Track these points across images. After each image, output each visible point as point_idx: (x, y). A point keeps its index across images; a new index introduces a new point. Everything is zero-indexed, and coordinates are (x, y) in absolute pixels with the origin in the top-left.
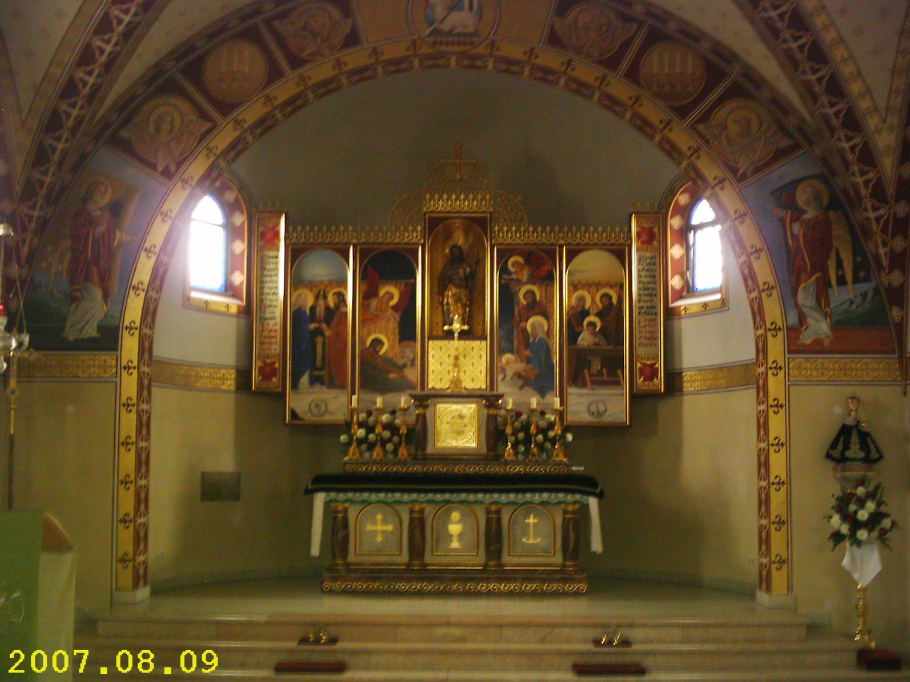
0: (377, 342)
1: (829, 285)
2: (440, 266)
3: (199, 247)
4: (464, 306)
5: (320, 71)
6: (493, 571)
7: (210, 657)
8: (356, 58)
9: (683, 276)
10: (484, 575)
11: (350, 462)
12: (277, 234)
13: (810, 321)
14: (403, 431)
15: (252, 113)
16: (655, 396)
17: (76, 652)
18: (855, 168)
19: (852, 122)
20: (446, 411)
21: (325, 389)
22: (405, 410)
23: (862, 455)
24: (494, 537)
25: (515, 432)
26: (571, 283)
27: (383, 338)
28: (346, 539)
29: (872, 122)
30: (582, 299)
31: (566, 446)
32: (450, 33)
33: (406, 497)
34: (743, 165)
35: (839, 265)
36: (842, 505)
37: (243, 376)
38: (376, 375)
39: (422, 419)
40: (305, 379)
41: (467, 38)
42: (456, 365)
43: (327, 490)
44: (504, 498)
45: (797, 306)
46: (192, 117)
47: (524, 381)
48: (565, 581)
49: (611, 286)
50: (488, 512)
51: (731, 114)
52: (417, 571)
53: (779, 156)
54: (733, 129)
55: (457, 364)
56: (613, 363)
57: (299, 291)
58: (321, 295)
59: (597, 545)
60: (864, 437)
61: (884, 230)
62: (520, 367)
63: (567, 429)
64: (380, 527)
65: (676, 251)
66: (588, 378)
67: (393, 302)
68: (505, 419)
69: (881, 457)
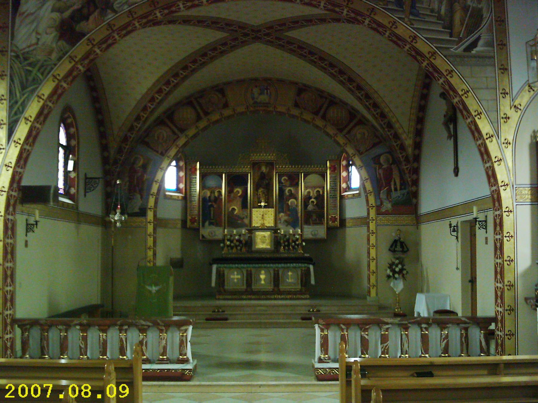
2: (256, 180)
3: (170, 178)
4: (266, 195)
5: (215, 117)
6: (277, 290)
7: (124, 389)
8: (227, 112)
9: (347, 183)
10: (273, 292)
12: (196, 170)
14: (244, 242)
15: (191, 132)
16: (336, 228)
18: (399, 152)
19: (396, 136)
20: (259, 234)
21: (214, 227)
23: (401, 249)
24: (276, 279)
25: (284, 242)
26: (305, 187)
27: (236, 208)
28: (224, 281)
29: (404, 136)
30: (309, 192)
31: (303, 247)
33: (245, 266)
35: (395, 184)
36: (391, 266)
37: (184, 222)
38: (233, 222)
40: (207, 223)
41: (266, 105)
43: (218, 263)
44: (280, 266)
45: (380, 198)
47: (288, 223)
48: (302, 294)
49: (320, 188)
50: (274, 270)
51: (359, 132)
52: (250, 291)
53: (375, 145)
54: (359, 136)
55: (263, 217)
56: (321, 216)
57: (205, 191)
58: (212, 192)
59: (313, 282)
60: (402, 244)
61: (409, 173)
64: (236, 277)
65: (344, 174)
66: (311, 222)
67: (239, 195)
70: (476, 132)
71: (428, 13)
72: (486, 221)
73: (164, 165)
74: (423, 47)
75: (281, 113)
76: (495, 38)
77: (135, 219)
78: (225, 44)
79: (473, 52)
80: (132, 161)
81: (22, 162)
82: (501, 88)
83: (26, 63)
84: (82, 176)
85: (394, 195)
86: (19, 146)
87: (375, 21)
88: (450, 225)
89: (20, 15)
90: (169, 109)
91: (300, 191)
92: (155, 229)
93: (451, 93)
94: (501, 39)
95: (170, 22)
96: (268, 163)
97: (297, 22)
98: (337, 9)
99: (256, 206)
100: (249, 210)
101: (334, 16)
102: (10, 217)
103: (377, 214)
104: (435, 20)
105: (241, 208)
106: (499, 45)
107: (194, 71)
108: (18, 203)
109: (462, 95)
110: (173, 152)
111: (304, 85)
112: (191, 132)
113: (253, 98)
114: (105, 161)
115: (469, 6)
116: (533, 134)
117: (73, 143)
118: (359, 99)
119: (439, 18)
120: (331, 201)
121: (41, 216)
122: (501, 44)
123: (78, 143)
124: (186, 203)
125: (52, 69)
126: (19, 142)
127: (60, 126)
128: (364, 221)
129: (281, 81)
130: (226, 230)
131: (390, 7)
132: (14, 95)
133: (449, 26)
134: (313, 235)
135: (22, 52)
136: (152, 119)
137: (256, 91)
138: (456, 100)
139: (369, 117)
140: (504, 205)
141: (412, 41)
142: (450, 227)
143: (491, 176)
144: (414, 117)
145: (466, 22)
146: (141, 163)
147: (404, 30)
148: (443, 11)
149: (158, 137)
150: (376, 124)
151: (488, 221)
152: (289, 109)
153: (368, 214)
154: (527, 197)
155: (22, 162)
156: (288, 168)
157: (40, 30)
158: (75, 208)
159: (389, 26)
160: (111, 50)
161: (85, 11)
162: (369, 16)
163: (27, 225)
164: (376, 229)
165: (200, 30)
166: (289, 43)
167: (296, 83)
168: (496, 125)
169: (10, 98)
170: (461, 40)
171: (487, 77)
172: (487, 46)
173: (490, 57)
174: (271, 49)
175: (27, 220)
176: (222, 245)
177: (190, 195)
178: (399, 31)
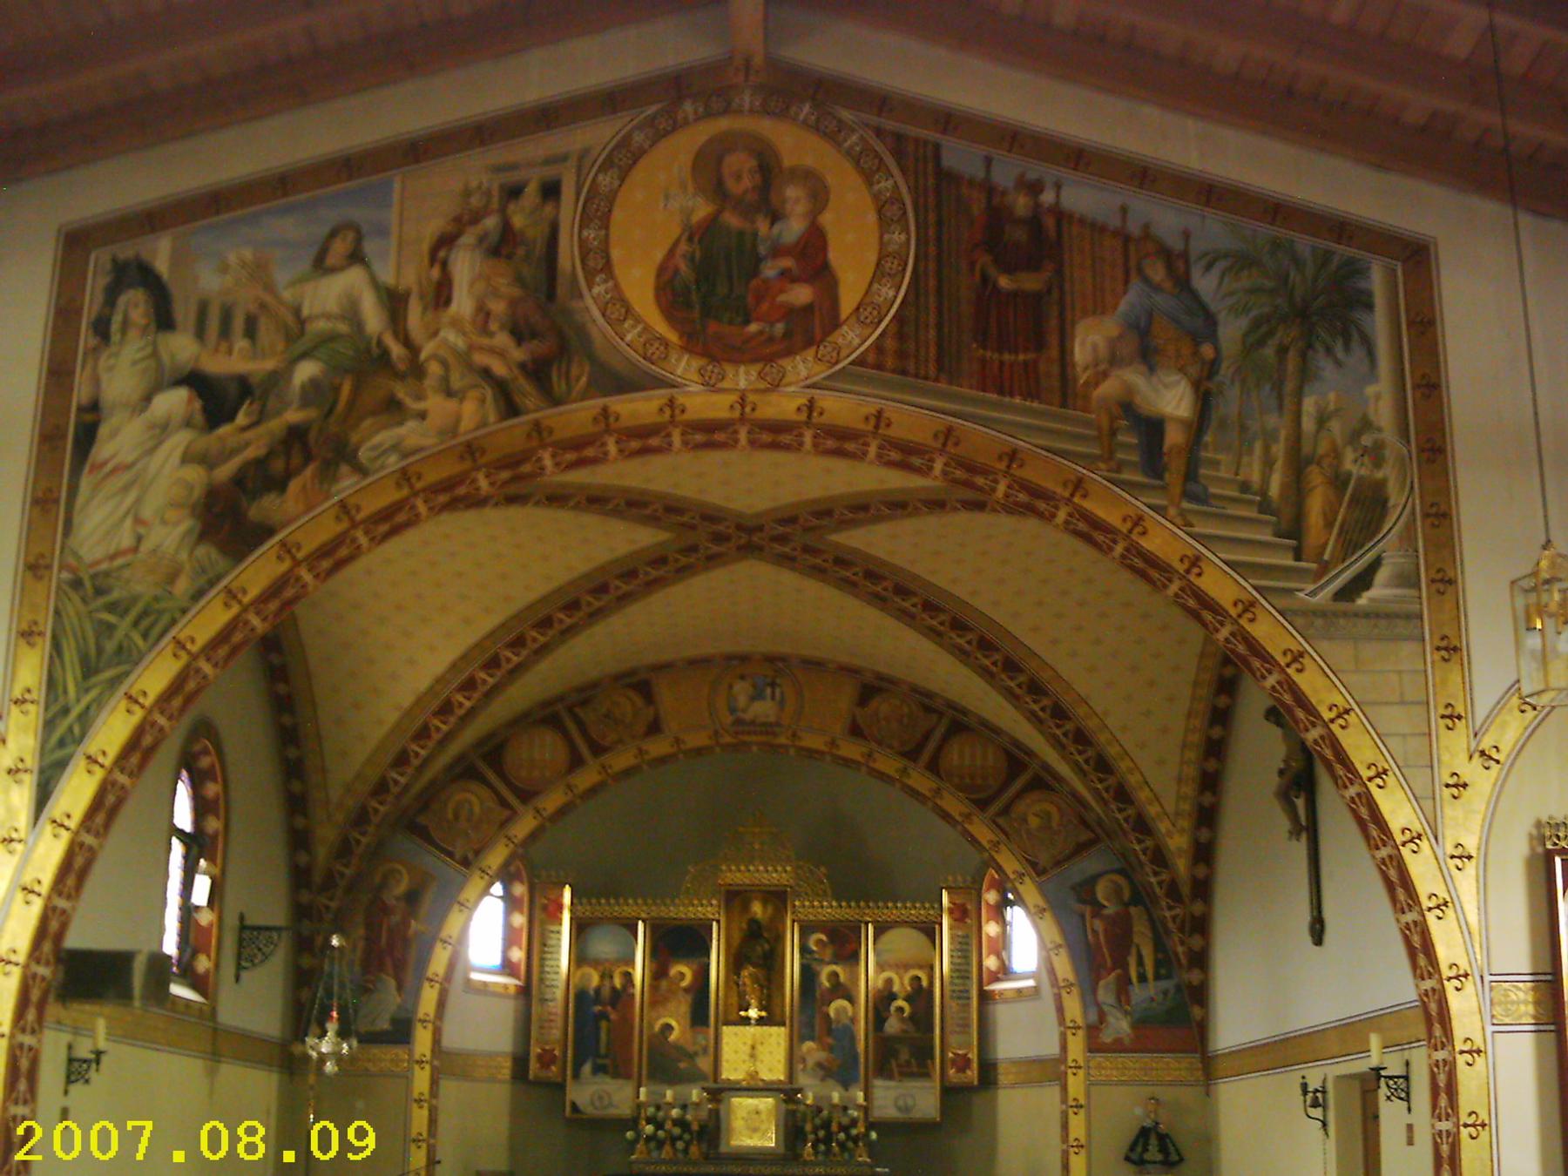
0: (668, 1028)
1: (1130, 982)
4: (762, 987)
5: (621, 760)
7: (361, 1133)
8: (658, 747)
9: (999, 956)
11: (637, 1162)
12: (560, 907)
13: (1111, 1019)
14: (695, 1127)
15: (552, 801)
16: (966, 1089)
17: (130, 1124)
18: (1148, 869)
19: (1143, 826)
20: (742, 1105)
21: (608, 1080)
22: (697, 1105)
23: (1159, 1157)
25: (815, 1130)
27: (674, 1023)
29: (1163, 827)
30: (889, 982)
31: (870, 1145)
32: (753, 723)
34: (1044, 859)
35: (1140, 962)
37: (520, 1063)
39: (715, 1115)
40: (587, 1068)
41: (769, 728)
42: (753, 1056)
45: (1098, 1005)
46: (491, 803)
47: (825, 1072)
49: (921, 967)
51: (1034, 810)
53: (1080, 849)
54: (1034, 822)
55: (753, 1050)
56: (923, 1053)
58: (606, 975)
60: (1163, 1139)
61: (1181, 929)
62: (822, 1055)
63: (871, 1126)
65: (991, 929)
66: (896, 1070)
67: (684, 984)
68: (804, 1115)
69: (1181, 1160)
70: (1371, 823)
71: (1235, 494)
72: (1406, 1078)
73: (469, 893)
74: (1220, 585)
75: (811, 753)
76: (1422, 562)
77: (375, 1050)
78: (660, 561)
79: (1363, 601)
80: (377, 880)
81: (71, 881)
82: (1442, 701)
83: (102, 601)
84: (232, 921)
85: (1138, 993)
86: (65, 836)
87: (1087, 517)
88: (1304, 1087)
89: (91, 471)
90: (491, 735)
91: (863, 976)
92: (434, 1083)
93: (1300, 714)
94: (1438, 566)
95: (511, 500)
96: (769, 892)
97: (865, 508)
98: (980, 481)
99: (733, 1017)
100: (712, 1030)
101: (970, 495)
102: (27, 1040)
103: (1090, 1051)
104: (1251, 513)
105: (688, 1021)
106: (1433, 581)
107: (569, 632)
108: (51, 999)
109: (1332, 721)
110: (496, 857)
111: (880, 677)
112: (552, 801)
113: (732, 710)
114: (300, 877)
115: (1349, 475)
116: (1535, 832)
117: (213, 824)
118: (1033, 717)
119: (1265, 506)
120: (953, 1006)
121: (110, 1036)
122: (1441, 581)
123: (227, 827)
124: (528, 1006)
125: (174, 622)
126: (67, 822)
127: (177, 777)
128: (1051, 1071)
129: (814, 665)
130: (642, 1090)
131: (1125, 476)
132: (60, 689)
133: (1293, 530)
134: (899, 1109)
135: (92, 571)
136: (445, 758)
137: (742, 690)
138: (1313, 734)
139: (1064, 769)
140: (1459, 1033)
141: (1188, 571)
142: (1305, 1092)
143: (1420, 950)
144: (1192, 771)
145: (1340, 518)
146: (402, 887)
147: (1164, 540)
148: (1274, 490)
149: (456, 816)
150: (1080, 788)
151: (1414, 1078)
152: (833, 743)
153: (1064, 1047)
154: (1522, 1008)
155: (71, 881)
156: (830, 910)
157: (147, 512)
158: (209, 1014)
159: (1124, 528)
160: (349, 572)
161: (278, 465)
162: (1069, 501)
163: (71, 1061)
164: (1088, 1095)
165: (591, 523)
166: (840, 562)
167: (850, 671)
168: (1427, 804)
169: (48, 695)
170: (1324, 568)
171: (1400, 672)
172: (1398, 586)
173: (1408, 617)
174: (789, 579)
175: (70, 1047)
176: (629, 1135)
177: (542, 980)
178: (1151, 544)
